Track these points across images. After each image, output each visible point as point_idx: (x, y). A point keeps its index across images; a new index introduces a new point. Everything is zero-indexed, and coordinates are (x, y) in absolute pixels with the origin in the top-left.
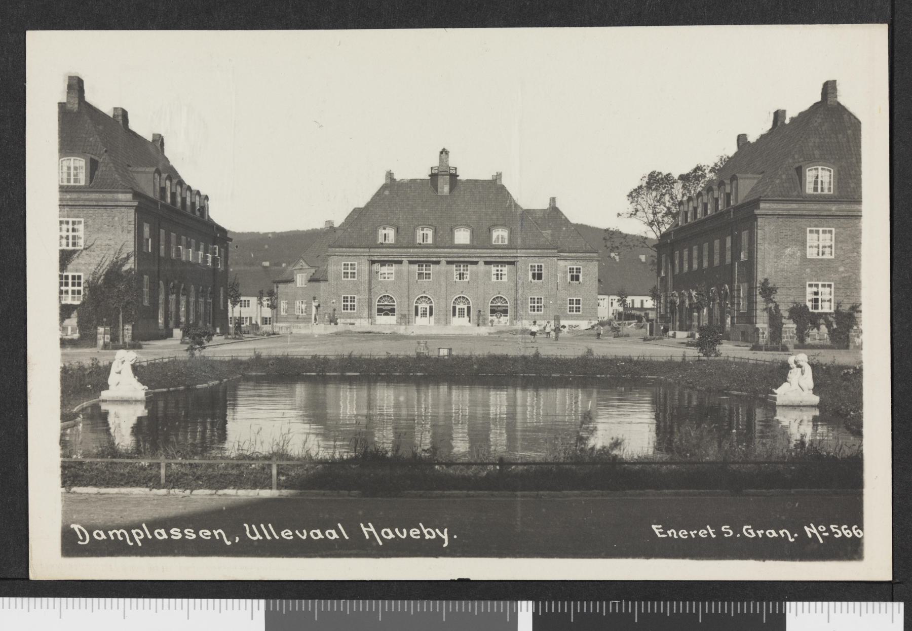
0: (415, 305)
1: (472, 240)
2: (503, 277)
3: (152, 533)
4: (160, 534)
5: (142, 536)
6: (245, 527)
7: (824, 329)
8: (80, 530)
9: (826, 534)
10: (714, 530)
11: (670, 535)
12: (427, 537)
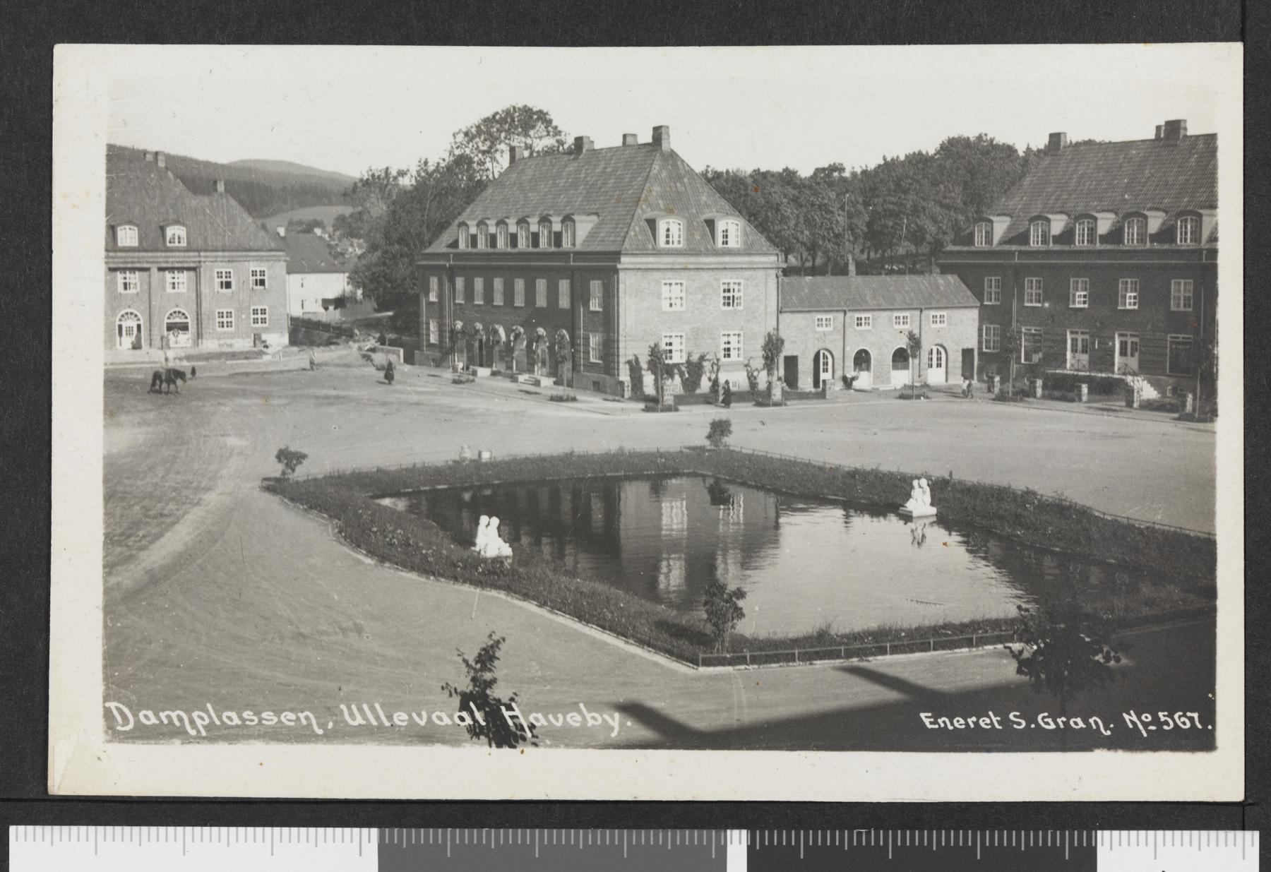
0: (118, 323)
1: (141, 239)
2: (180, 286)
3: (220, 718)
4: (146, 717)
5: (207, 721)
6: (342, 711)
7: (677, 379)
8: (118, 709)
9: (1152, 728)
10: (999, 719)
11: (942, 725)
12: (590, 723)
